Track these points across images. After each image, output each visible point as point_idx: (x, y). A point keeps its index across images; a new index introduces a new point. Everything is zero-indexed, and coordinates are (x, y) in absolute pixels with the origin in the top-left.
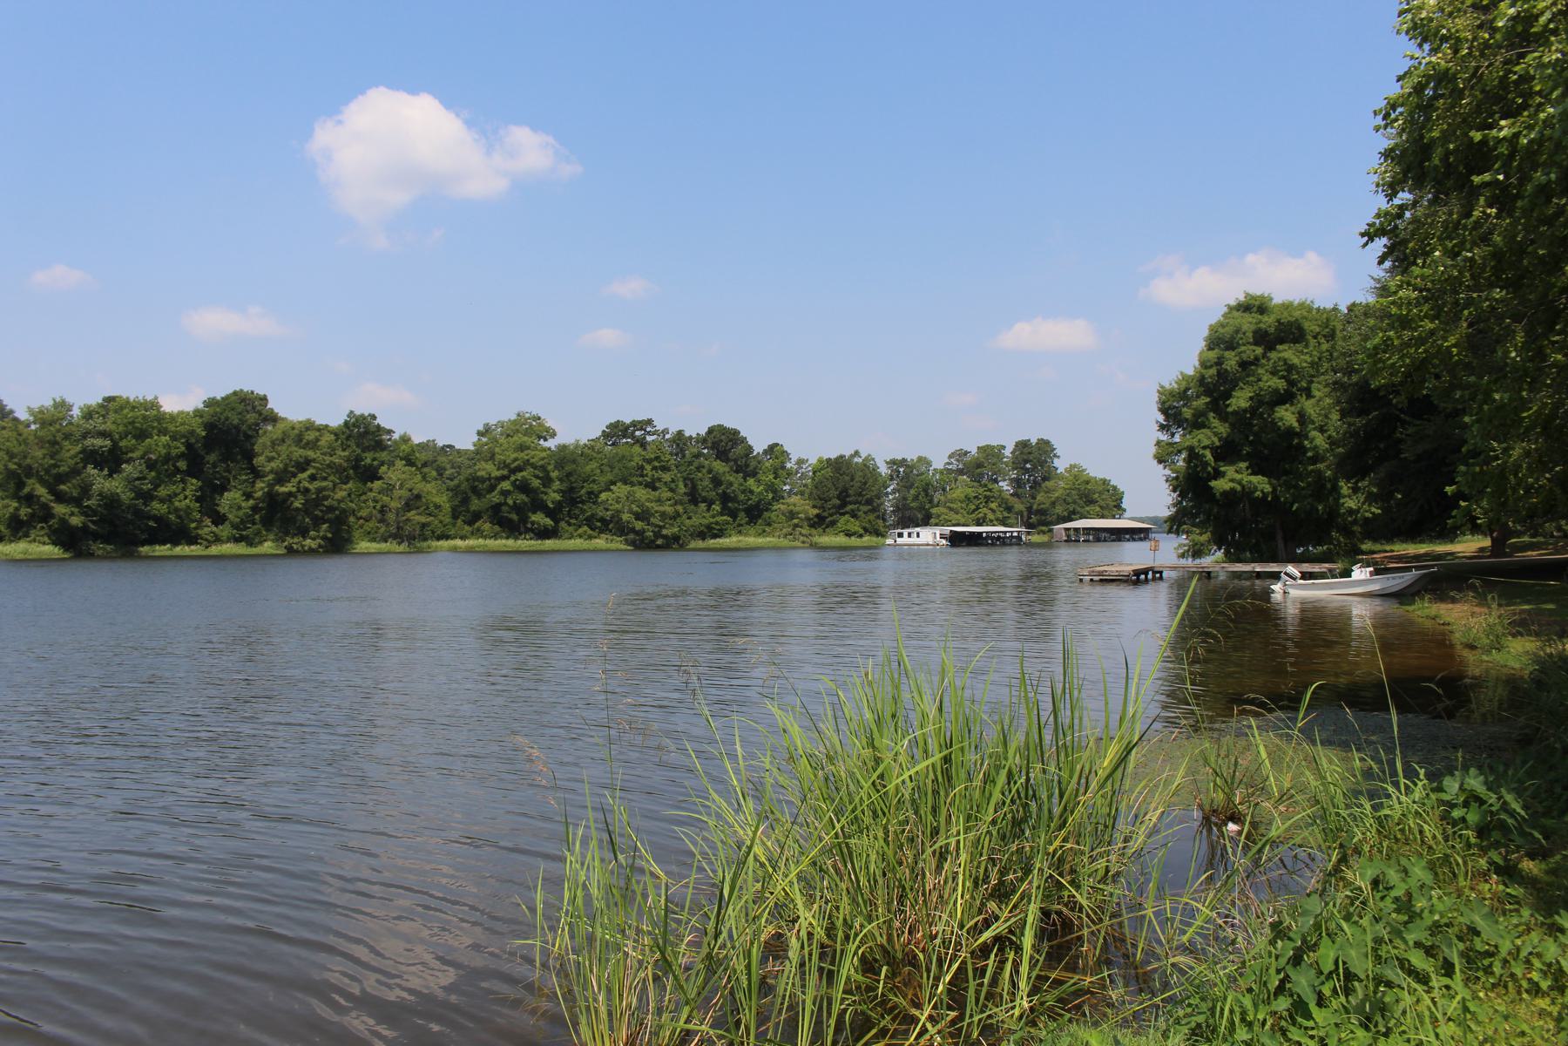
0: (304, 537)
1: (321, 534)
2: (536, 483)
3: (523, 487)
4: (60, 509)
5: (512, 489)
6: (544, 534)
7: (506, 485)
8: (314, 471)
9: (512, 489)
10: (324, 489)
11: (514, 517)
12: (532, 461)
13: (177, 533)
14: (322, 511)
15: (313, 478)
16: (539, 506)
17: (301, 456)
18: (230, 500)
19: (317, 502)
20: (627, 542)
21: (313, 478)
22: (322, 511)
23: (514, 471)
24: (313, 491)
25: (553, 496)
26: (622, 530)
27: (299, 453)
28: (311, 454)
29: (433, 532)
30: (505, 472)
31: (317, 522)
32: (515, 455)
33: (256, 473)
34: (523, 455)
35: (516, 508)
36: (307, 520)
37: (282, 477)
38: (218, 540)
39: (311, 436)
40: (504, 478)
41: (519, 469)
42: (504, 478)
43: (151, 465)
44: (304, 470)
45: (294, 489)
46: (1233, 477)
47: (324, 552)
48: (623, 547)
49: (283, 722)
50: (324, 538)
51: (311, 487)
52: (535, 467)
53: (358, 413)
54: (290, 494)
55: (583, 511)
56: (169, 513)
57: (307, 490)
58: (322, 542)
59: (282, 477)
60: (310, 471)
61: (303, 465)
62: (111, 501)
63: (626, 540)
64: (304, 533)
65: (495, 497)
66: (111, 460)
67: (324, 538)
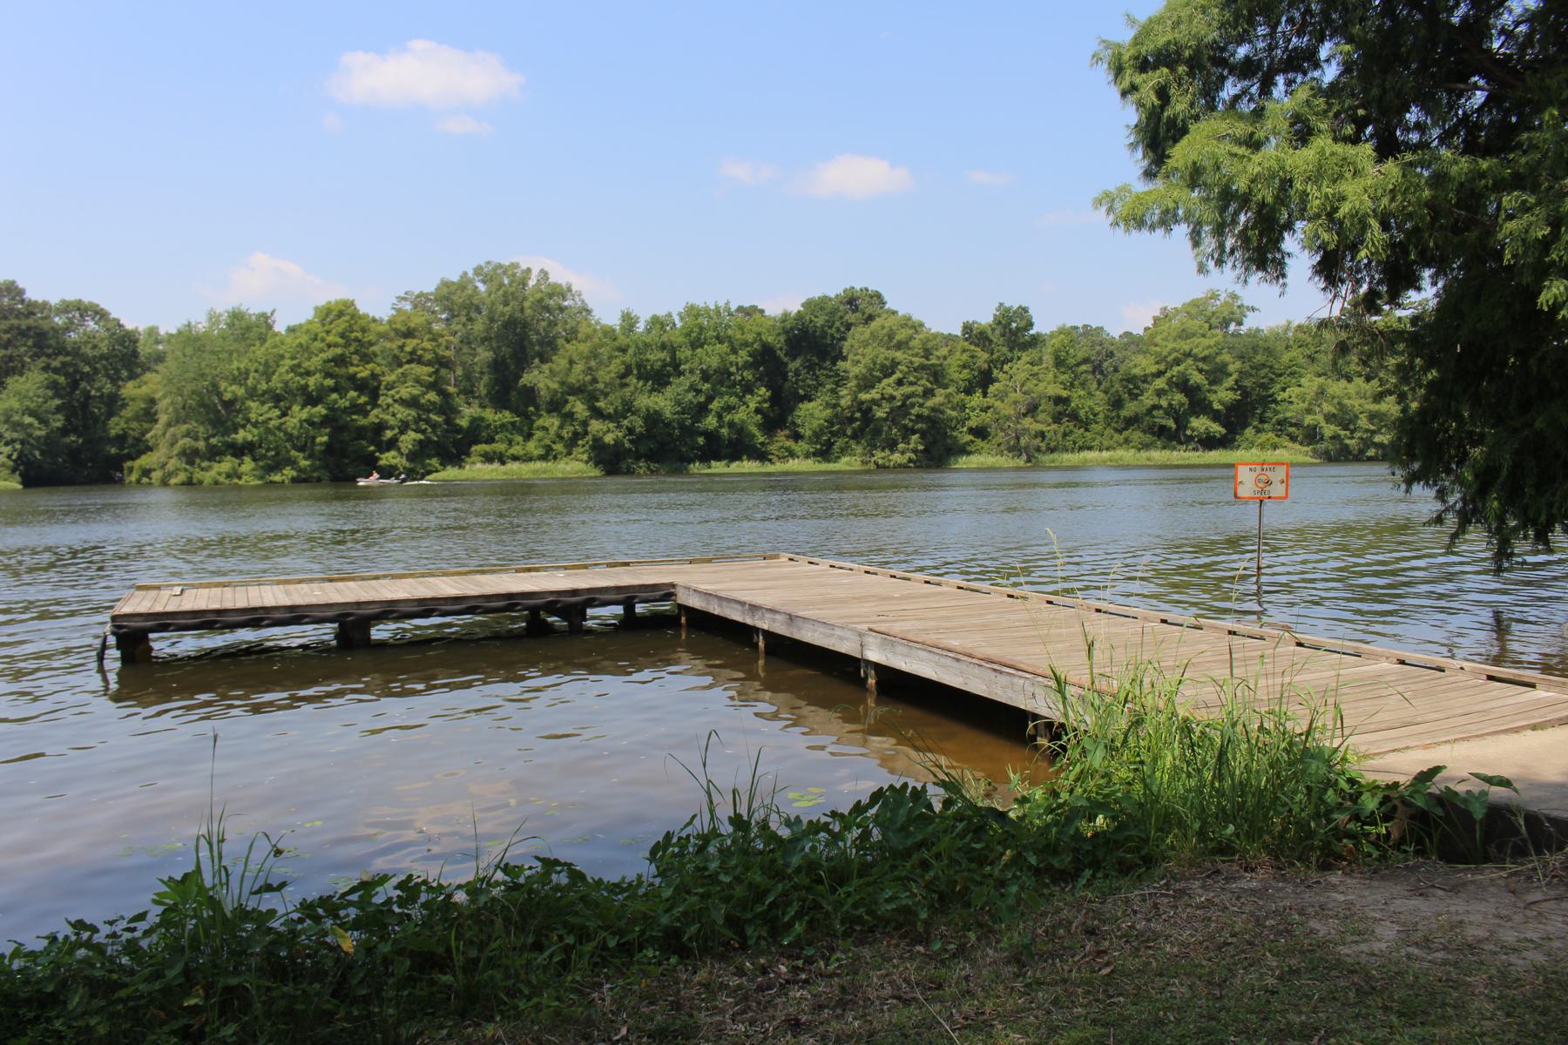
0: (892, 451)
1: (911, 446)
2: (1197, 378)
3: (1183, 385)
4: (596, 426)
5: (1166, 387)
6: (1209, 443)
7: (1160, 383)
8: (901, 376)
9: (1166, 387)
10: (912, 395)
11: (1171, 424)
12: (1195, 351)
13: (737, 447)
14: (911, 420)
15: (900, 383)
16: (1198, 404)
17: (886, 359)
18: (812, 414)
19: (904, 408)
20: (1315, 453)
21: (900, 383)
22: (911, 420)
23: (1170, 366)
24: (899, 397)
25: (1222, 396)
26: (1311, 436)
27: (884, 355)
28: (899, 355)
29: (1075, 443)
30: (1162, 367)
31: (907, 432)
32: (1171, 345)
33: (840, 380)
34: (1185, 346)
35: (1171, 411)
36: (895, 431)
37: (867, 383)
38: (792, 455)
39: (901, 335)
40: (1159, 374)
41: (1177, 362)
42: (1159, 374)
43: (706, 377)
44: (890, 375)
45: (878, 396)
46: (125, 373)
47: (916, 467)
48: (1309, 459)
49: (12, 717)
50: (915, 451)
51: (895, 393)
52: (1196, 359)
53: (1007, 305)
54: (874, 401)
55: (1276, 412)
56: (721, 427)
57: (892, 398)
58: (913, 456)
59: (867, 383)
60: (898, 375)
61: (889, 370)
62: (653, 418)
63: (1314, 451)
64: (892, 445)
65: (1148, 399)
66: (658, 379)
67: (915, 451)
